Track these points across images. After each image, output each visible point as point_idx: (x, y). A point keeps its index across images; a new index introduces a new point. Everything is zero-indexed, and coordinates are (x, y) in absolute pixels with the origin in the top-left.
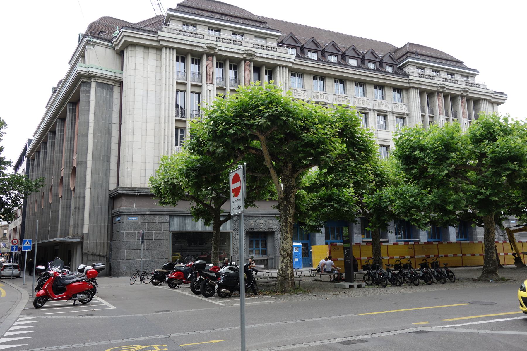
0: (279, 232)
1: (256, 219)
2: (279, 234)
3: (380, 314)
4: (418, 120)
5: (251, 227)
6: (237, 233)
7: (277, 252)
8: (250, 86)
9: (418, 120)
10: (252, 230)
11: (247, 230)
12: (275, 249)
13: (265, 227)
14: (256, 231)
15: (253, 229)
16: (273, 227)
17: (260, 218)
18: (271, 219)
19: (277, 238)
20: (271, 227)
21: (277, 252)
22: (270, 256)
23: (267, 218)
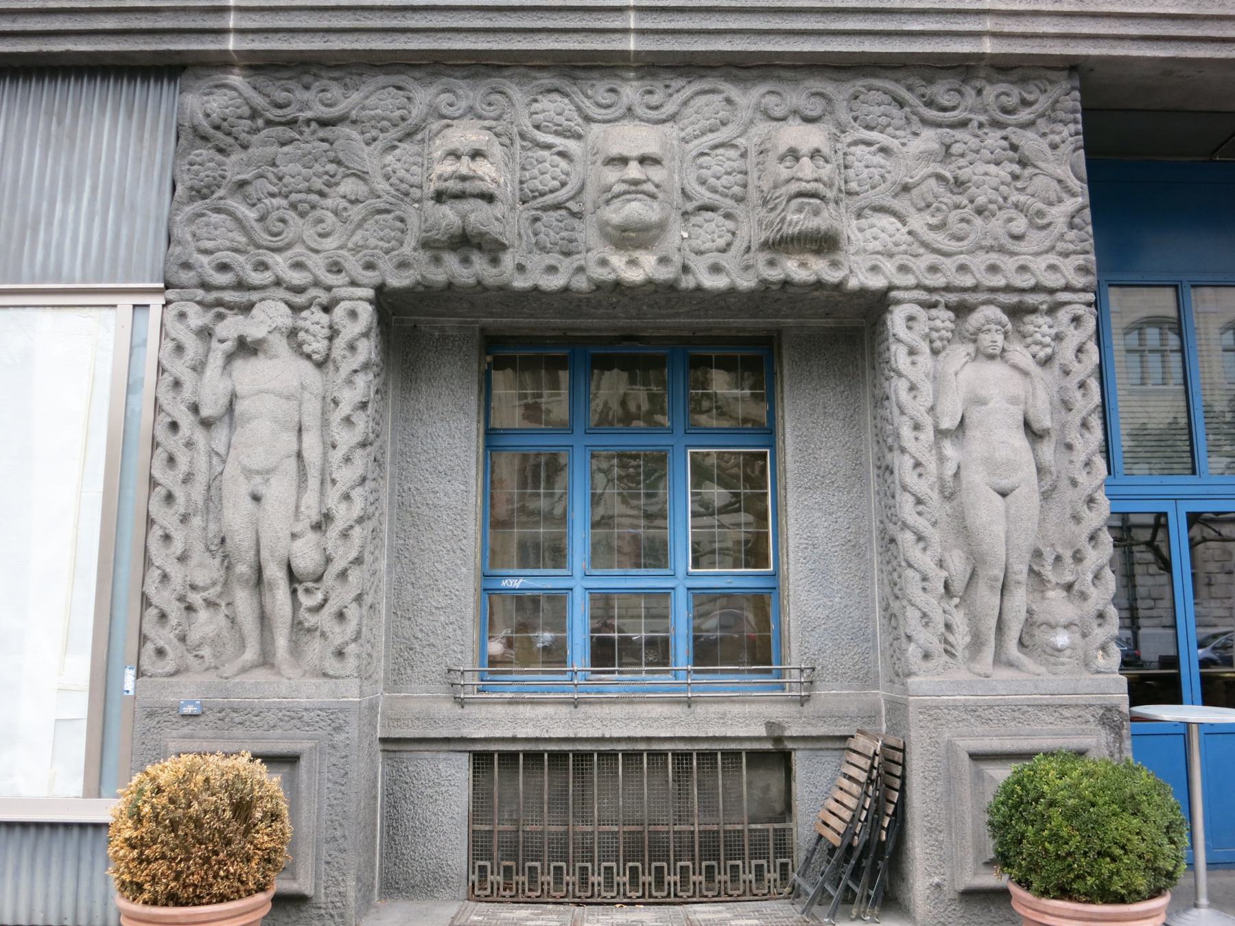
0: (961, 310)
1: (552, 107)
2: (959, 336)
3: (375, 842)
4: (61, 897)
5: (449, 216)
6: (232, 326)
7: (926, 637)
8: (364, 145)
9: (61, 897)
10: (480, 268)
11: (398, 281)
12: (896, 591)
13: (711, 230)
14: (553, 283)
15: (493, 249)
16: (849, 228)
17: (631, 91)
18: (814, 107)
19: (917, 407)
20: (799, 220)
21: (926, 637)
22: (828, 693)
23: (748, 97)
